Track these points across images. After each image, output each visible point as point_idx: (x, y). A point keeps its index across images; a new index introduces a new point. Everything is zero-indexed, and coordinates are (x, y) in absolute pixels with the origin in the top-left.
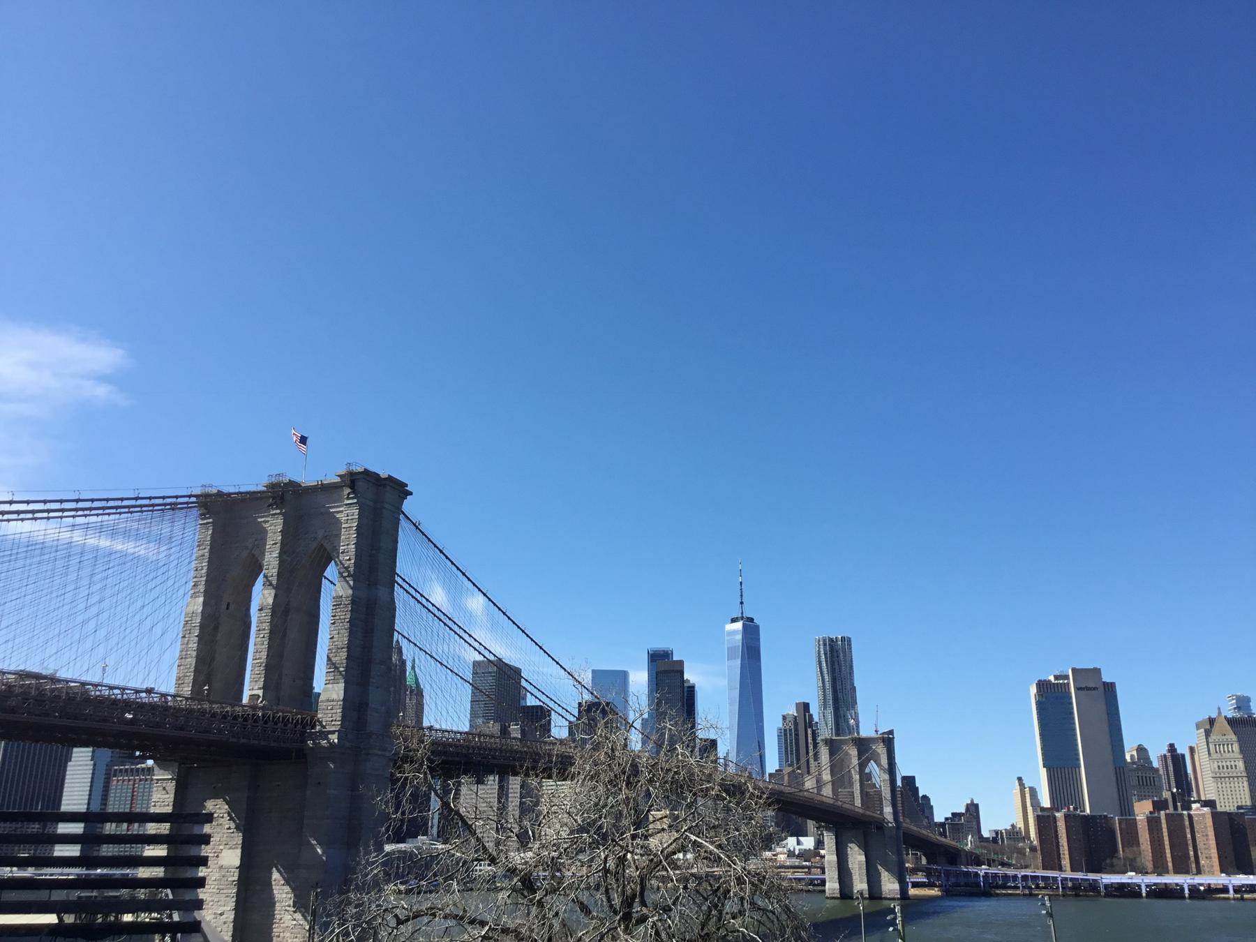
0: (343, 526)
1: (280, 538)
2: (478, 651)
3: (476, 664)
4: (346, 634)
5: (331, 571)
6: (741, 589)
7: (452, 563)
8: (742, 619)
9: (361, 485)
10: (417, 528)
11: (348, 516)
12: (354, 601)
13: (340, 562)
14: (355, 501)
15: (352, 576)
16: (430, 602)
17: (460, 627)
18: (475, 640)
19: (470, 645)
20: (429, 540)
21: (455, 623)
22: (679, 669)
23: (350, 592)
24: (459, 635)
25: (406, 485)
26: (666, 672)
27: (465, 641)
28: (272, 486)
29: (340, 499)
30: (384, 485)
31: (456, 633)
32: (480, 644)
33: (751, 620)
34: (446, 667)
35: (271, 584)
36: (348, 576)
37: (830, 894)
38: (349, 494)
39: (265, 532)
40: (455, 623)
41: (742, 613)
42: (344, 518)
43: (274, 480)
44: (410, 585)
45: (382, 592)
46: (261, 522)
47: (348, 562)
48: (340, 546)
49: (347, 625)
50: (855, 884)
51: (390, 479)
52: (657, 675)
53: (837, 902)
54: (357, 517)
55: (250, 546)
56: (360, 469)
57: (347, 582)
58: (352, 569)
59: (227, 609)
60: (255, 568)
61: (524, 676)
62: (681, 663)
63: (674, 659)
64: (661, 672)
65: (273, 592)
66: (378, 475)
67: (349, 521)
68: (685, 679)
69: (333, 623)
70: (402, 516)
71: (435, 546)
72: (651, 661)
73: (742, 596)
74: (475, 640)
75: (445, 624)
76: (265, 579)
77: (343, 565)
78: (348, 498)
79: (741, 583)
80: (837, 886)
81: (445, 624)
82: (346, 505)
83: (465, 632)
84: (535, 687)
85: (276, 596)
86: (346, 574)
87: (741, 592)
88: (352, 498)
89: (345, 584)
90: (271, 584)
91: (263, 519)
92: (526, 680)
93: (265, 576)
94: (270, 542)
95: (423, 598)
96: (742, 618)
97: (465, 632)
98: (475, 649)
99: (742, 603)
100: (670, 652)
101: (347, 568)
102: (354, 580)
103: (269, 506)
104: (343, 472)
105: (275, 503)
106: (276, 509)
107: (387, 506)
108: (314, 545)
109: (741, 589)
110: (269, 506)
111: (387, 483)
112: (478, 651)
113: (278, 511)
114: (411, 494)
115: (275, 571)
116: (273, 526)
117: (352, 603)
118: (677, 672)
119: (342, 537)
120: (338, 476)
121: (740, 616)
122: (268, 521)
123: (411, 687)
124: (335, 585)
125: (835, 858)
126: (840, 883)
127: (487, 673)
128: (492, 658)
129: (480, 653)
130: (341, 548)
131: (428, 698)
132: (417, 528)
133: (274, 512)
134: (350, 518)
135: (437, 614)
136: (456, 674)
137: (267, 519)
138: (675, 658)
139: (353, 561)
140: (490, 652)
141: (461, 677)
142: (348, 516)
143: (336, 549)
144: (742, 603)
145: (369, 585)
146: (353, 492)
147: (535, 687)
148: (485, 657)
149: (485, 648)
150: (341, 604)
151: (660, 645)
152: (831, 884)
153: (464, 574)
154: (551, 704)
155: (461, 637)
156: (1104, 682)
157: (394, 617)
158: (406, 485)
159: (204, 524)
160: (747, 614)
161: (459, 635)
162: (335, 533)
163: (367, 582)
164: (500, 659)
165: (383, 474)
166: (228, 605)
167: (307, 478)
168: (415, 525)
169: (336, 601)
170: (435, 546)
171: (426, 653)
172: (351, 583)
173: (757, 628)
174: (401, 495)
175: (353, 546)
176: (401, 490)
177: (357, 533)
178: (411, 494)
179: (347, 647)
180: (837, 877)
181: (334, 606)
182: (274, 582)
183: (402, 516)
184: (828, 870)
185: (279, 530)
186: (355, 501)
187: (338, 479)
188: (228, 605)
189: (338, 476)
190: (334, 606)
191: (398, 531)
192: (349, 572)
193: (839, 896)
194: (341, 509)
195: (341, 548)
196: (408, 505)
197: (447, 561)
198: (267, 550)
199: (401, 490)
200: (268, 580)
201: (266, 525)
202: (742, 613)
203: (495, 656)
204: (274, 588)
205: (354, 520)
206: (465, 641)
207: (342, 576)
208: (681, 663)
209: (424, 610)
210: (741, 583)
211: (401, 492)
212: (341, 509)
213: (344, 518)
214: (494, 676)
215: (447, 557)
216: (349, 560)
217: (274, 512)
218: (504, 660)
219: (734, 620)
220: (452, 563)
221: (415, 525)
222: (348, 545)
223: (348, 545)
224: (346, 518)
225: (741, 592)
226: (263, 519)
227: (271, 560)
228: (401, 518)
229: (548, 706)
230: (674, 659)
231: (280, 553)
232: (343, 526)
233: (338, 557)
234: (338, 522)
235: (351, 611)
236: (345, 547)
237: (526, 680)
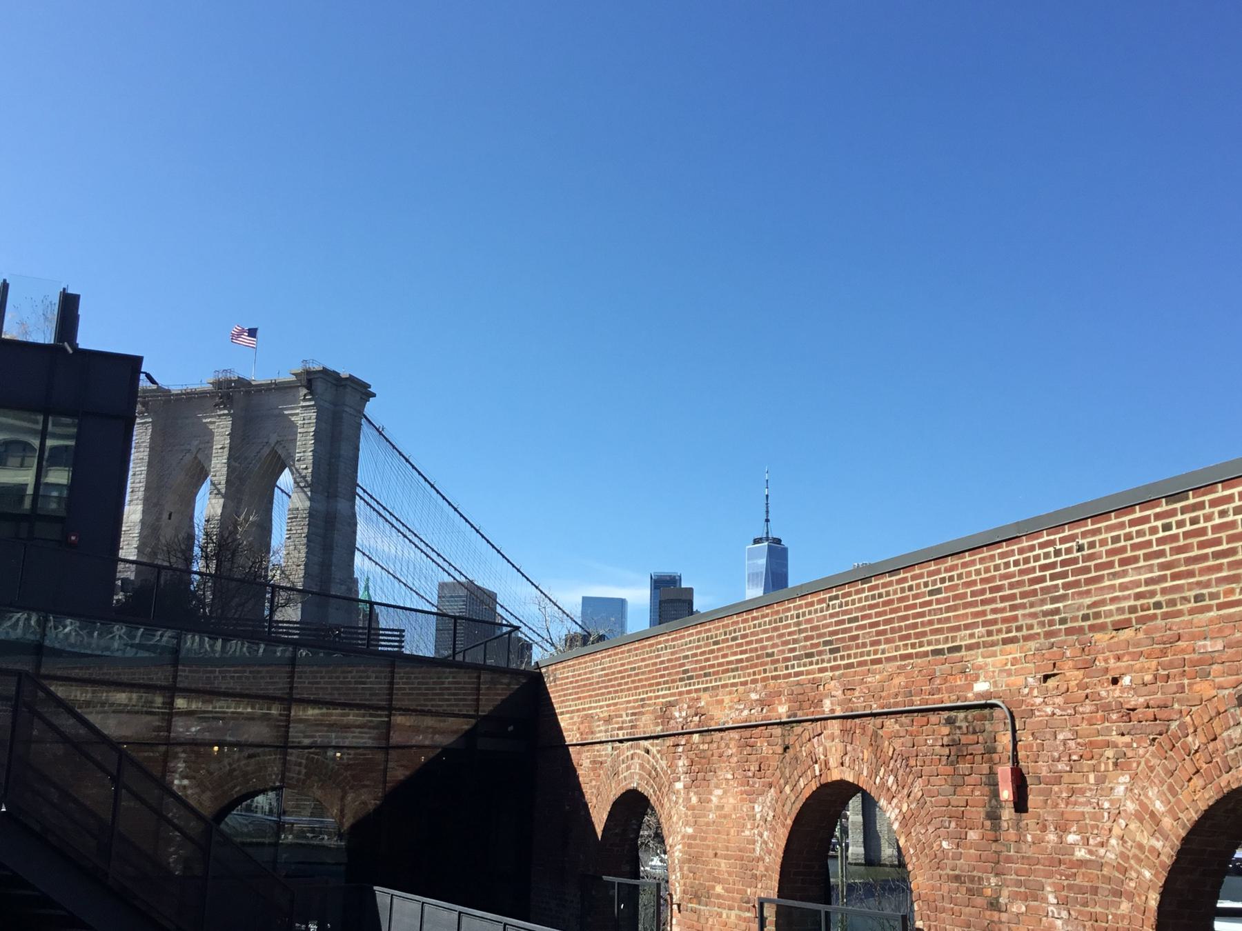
0: (299, 430)
1: (228, 441)
2: (447, 572)
3: (442, 586)
4: (304, 550)
5: (286, 479)
6: (767, 504)
7: (420, 473)
8: (767, 540)
9: (319, 386)
10: (381, 433)
11: (304, 420)
12: (312, 514)
13: (297, 470)
14: (313, 403)
15: (309, 486)
16: (394, 516)
17: (427, 545)
18: (444, 560)
19: (439, 565)
20: (394, 447)
21: (422, 540)
22: (688, 598)
23: (308, 504)
24: (425, 554)
25: (370, 387)
26: (672, 601)
27: (433, 561)
28: (218, 384)
29: (296, 401)
30: (345, 386)
31: (422, 551)
32: (450, 564)
33: (778, 541)
34: (411, 589)
35: (219, 493)
36: (305, 487)
37: (853, 859)
38: (305, 395)
39: (211, 434)
40: (422, 540)
41: (767, 533)
42: (300, 422)
43: (221, 376)
44: (371, 497)
45: (342, 505)
46: (207, 423)
47: (305, 471)
48: (295, 453)
49: (305, 541)
50: (882, 849)
51: (351, 379)
52: (660, 604)
53: (863, 868)
54: (315, 421)
55: (194, 450)
56: (317, 368)
57: (305, 493)
58: (309, 479)
59: (170, 519)
60: (200, 473)
61: (360, 484)
62: (691, 590)
63: (683, 586)
64: (665, 602)
65: (222, 501)
66: (338, 374)
67: (305, 426)
68: (694, 610)
69: (289, 538)
70: (363, 421)
71: (400, 454)
72: (655, 588)
73: (767, 512)
74: (444, 560)
75: (410, 541)
76: (213, 487)
77: (300, 474)
78: (305, 400)
79: (767, 496)
80: (861, 850)
81: (410, 541)
82: (303, 407)
83: (433, 550)
84: (512, 614)
85: (224, 507)
86: (302, 485)
87: (767, 508)
88: (310, 400)
89: (302, 495)
90: (219, 493)
91: (209, 420)
92: (502, 606)
93: (213, 483)
94: (217, 446)
95: (428, 548)
96: (767, 539)
97: (433, 550)
98: (444, 570)
99: (767, 520)
100: (677, 578)
101: (304, 477)
102: (311, 491)
103: (215, 406)
104: (299, 369)
105: (222, 403)
106: (225, 408)
107: (347, 409)
108: (266, 451)
109: (767, 504)
110: (215, 406)
111: (349, 383)
112: (447, 572)
113: (226, 412)
114: (374, 395)
115: (223, 479)
116: (221, 428)
117: (309, 517)
118: (684, 601)
119: (298, 443)
120: (293, 374)
121: (765, 536)
122: (214, 422)
123: (364, 610)
124: (290, 497)
125: (860, 818)
126: (865, 847)
127: (456, 597)
128: (463, 579)
129: (449, 574)
130: (297, 455)
131: (434, 594)
132: (381, 433)
133: (222, 412)
134: (306, 422)
135: (376, 508)
136: (422, 597)
137: (213, 420)
138: (683, 586)
139: (310, 470)
140: (461, 573)
141: (428, 601)
142: (304, 420)
143: (292, 457)
144: (767, 520)
145: (328, 497)
146: (311, 393)
147: (512, 614)
148: (454, 578)
149: (456, 569)
150: (297, 517)
151: (666, 569)
152: (855, 848)
153: (432, 486)
154: (535, 637)
155: (428, 556)
156: (764, 593)
157: (355, 532)
158: (370, 387)
159: (142, 423)
160: (774, 534)
161: (425, 554)
162: (290, 438)
163: (326, 494)
164: (472, 582)
165: (344, 374)
166: (170, 515)
167: (257, 375)
168: (378, 430)
169: (293, 514)
170: (400, 454)
171: (389, 573)
172: (309, 493)
173: (785, 550)
174: (364, 397)
175: (311, 454)
176: (363, 392)
177: (315, 439)
178: (374, 395)
179: (305, 565)
180: (861, 840)
181: (289, 519)
182: (223, 491)
183: (363, 421)
184: (852, 833)
185: (227, 433)
186: (313, 403)
187: (293, 378)
188: (170, 515)
189: (293, 374)
190: (289, 519)
191: (359, 438)
192: (306, 481)
193: (863, 862)
194: (297, 411)
195: (297, 455)
196: (370, 408)
197: (414, 471)
198: (214, 455)
199: (363, 392)
200: (216, 488)
201: (211, 427)
202: (767, 533)
203: (466, 578)
204: (223, 497)
205: (312, 425)
206: (433, 561)
207: (299, 486)
208: (691, 590)
209: (387, 526)
210: (767, 496)
211: (363, 394)
212: (297, 411)
213: (300, 422)
214: (464, 601)
215: (413, 467)
216: (306, 468)
217: (222, 412)
218: (476, 583)
219: (756, 541)
220: (420, 473)
221: (378, 430)
222: (304, 452)
223: (304, 452)
224: (302, 422)
225: (767, 508)
226: (209, 420)
227: (219, 465)
228: (363, 422)
229: (526, 636)
230: (683, 586)
231: (228, 459)
232: (299, 430)
233: (294, 465)
234: (293, 426)
235: (308, 524)
236: (302, 454)
237: (502, 606)
